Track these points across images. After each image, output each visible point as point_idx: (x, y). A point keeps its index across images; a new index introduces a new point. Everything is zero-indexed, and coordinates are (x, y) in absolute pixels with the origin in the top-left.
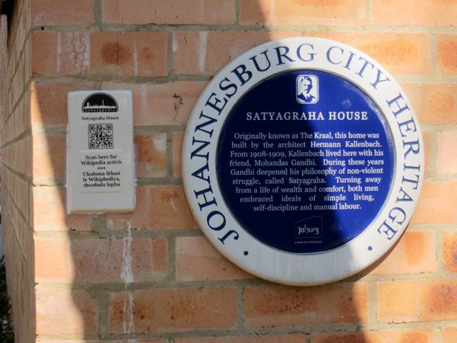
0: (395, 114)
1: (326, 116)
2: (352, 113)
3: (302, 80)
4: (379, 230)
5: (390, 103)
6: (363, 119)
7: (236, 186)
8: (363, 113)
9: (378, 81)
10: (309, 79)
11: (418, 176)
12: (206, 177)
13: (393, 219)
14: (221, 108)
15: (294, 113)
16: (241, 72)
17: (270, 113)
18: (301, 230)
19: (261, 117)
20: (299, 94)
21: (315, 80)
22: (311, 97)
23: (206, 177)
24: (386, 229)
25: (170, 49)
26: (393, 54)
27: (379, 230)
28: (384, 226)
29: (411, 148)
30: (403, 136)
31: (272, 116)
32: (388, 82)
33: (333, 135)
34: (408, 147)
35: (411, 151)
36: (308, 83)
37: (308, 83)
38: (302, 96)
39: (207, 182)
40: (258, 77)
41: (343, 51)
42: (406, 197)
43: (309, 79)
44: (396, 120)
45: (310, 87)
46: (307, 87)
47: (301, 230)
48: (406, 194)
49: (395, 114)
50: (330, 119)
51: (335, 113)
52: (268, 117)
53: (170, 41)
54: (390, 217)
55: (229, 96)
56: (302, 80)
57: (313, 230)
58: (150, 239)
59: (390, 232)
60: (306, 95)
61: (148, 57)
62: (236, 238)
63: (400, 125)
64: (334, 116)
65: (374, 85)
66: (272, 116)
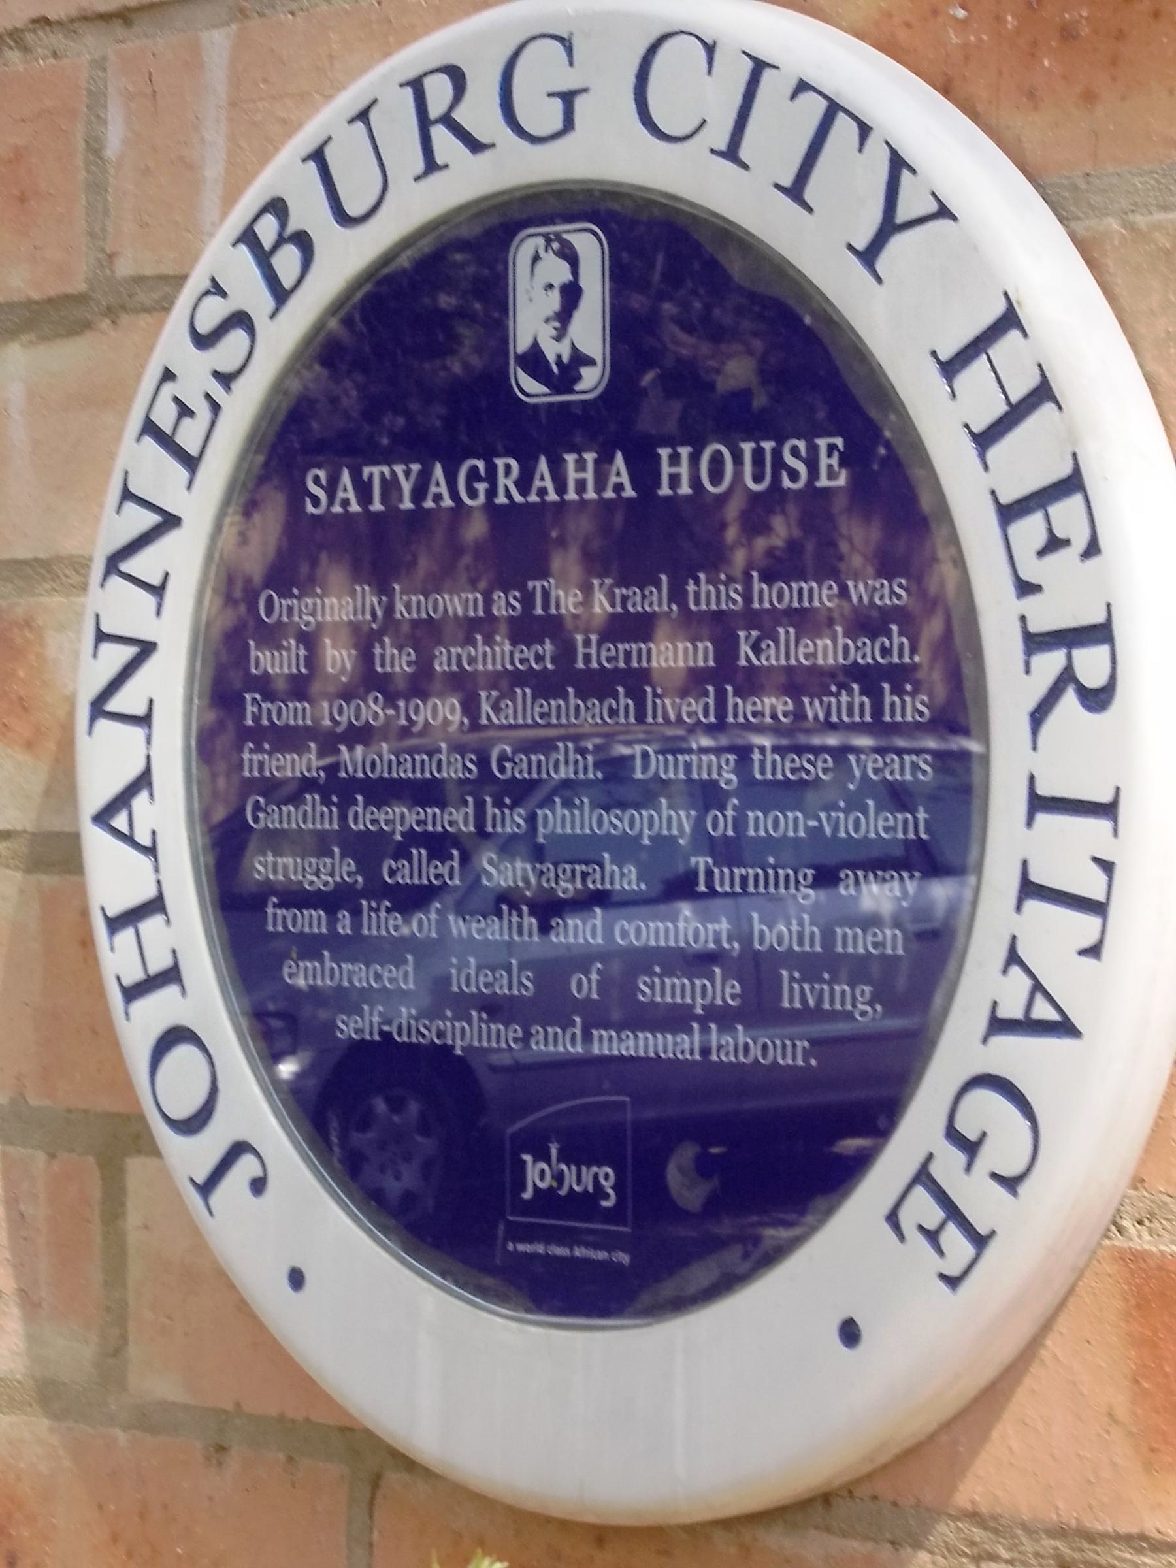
0: (985, 439)
1: (644, 471)
2: (768, 445)
3: (536, 258)
4: (893, 1218)
5: (950, 368)
6: (823, 482)
7: (267, 889)
8: (822, 443)
9: (889, 227)
10: (570, 256)
11: (1107, 867)
12: (1018, 981)
13: (970, 1148)
14: (1015, 529)
15: (500, 462)
16: (277, 241)
17: (399, 469)
18: (537, 1175)
19: (363, 490)
20: (522, 344)
21: (589, 246)
22: (579, 359)
23: (1018, 981)
24: (933, 1215)
25: (95, 148)
26: (1067, 34)
27: (893, 1218)
28: (919, 1192)
29: (1067, 676)
30: (1026, 588)
31: (406, 487)
32: (943, 224)
33: (677, 595)
34: (1051, 663)
35: (1070, 697)
36: (559, 272)
37: (559, 272)
38: (534, 361)
39: (145, 862)
40: (344, 259)
41: (710, 49)
42: (1043, 1011)
43: (570, 256)
44: (985, 481)
45: (571, 294)
46: (554, 301)
47: (537, 1175)
48: (1038, 987)
49: (985, 439)
50: (665, 490)
51: (684, 451)
52: (390, 486)
53: (97, 100)
54: (953, 1135)
55: (226, 379)
56: (536, 258)
57: (588, 1174)
58: (41, 1157)
59: (952, 1236)
60: (553, 350)
61: (22, 199)
62: (258, 1186)
63: (1009, 513)
64: (684, 470)
65: (869, 256)
66: (406, 487)
